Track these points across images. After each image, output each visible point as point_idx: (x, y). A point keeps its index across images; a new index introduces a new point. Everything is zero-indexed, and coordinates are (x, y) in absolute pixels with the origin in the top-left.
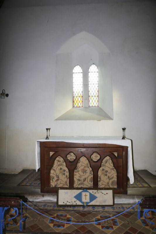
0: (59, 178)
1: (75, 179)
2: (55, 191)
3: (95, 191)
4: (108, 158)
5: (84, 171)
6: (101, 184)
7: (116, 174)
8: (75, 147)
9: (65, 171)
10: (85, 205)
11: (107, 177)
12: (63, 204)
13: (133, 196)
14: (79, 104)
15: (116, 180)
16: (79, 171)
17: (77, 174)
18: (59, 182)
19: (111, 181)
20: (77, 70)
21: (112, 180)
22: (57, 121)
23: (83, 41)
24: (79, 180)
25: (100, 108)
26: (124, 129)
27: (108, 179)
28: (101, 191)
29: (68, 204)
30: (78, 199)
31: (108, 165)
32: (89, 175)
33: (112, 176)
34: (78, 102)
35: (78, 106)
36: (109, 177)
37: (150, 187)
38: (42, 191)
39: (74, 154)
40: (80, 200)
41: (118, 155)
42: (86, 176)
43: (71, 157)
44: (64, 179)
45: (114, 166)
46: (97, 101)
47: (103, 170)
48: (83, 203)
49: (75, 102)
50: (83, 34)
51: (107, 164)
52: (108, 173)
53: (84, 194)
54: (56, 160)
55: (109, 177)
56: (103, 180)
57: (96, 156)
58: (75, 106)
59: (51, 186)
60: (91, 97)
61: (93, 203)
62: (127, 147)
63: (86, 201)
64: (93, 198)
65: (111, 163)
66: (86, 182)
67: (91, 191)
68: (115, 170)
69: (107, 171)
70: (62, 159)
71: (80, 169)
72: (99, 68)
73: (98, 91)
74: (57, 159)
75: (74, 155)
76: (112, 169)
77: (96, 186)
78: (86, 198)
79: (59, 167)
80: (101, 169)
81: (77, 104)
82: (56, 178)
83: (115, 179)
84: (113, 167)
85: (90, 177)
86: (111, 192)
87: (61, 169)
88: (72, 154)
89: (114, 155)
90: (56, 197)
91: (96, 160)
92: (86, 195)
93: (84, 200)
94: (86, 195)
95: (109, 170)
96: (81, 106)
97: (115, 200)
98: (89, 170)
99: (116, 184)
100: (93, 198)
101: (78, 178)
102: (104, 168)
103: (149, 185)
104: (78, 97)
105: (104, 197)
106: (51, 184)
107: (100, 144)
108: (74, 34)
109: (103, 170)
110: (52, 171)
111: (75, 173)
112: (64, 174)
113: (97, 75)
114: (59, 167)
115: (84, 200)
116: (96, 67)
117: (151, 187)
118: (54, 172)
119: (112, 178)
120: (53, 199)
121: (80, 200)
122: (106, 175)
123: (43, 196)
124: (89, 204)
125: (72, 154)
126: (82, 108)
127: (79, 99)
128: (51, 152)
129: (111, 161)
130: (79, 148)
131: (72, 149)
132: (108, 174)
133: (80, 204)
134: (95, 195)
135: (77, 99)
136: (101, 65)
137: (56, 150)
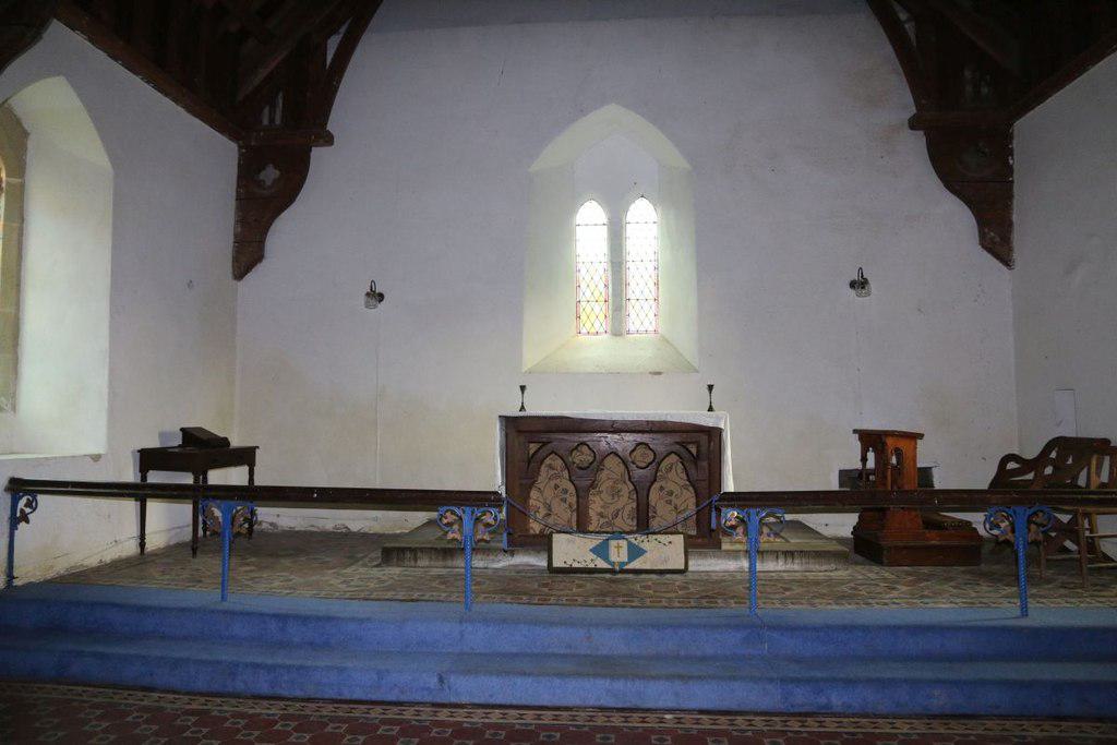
0: (550, 510)
1: (591, 513)
2: (543, 543)
3: (641, 538)
5: (616, 494)
6: (655, 524)
9: (565, 491)
10: (617, 568)
11: (671, 507)
12: (565, 566)
13: (734, 555)
14: (597, 325)
16: (601, 492)
17: (597, 499)
18: (550, 521)
20: (590, 219)
23: (612, 131)
24: (601, 515)
25: (663, 337)
26: (710, 388)
28: (655, 537)
29: (576, 565)
30: (599, 555)
31: (674, 478)
32: (626, 503)
34: (593, 318)
35: (593, 330)
38: (511, 543)
39: (590, 449)
40: (606, 558)
41: (697, 447)
42: (619, 505)
43: (582, 458)
44: (564, 513)
45: (689, 480)
46: (651, 316)
47: (662, 488)
48: (613, 564)
49: (583, 317)
50: (612, 111)
53: (613, 543)
54: (543, 468)
56: (663, 513)
57: (643, 455)
58: (584, 331)
59: (532, 532)
60: (633, 302)
61: (636, 564)
63: (618, 560)
64: (635, 552)
66: (618, 521)
67: (631, 538)
70: (559, 462)
71: (603, 488)
72: (659, 211)
73: (656, 284)
74: (548, 461)
75: (589, 452)
77: (644, 523)
78: (618, 553)
79: (552, 483)
80: (656, 485)
81: (588, 325)
82: (543, 511)
85: (628, 508)
86: (679, 540)
87: (556, 487)
88: (585, 448)
89: (690, 452)
90: (546, 556)
91: (643, 465)
92: (618, 547)
93: (614, 558)
94: (618, 547)
96: (602, 330)
97: (690, 563)
98: (627, 488)
100: (635, 552)
101: (599, 510)
102: (663, 483)
104: (592, 299)
105: (665, 551)
106: (531, 525)
107: (652, 422)
108: (583, 112)
109: (662, 488)
110: (534, 494)
111: (591, 497)
112: (564, 500)
113: (654, 230)
114: (552, 483)
115: (614, 558)
116: (651, 207)
118: (539, 494)
120: (539, 561)
121: (606, 558)
122: (670, 502)
123: (512, 554)
124: (626, 567)
125: (585, 448)
126: (605, 336)
127: (597, 309)
128: (532, 445)
130: (602, 435)
131: (586, 438)
133: (605, 565)
134: (642, 546)
135: (588, 310)
136: (663, 198)
137: (544, 440)
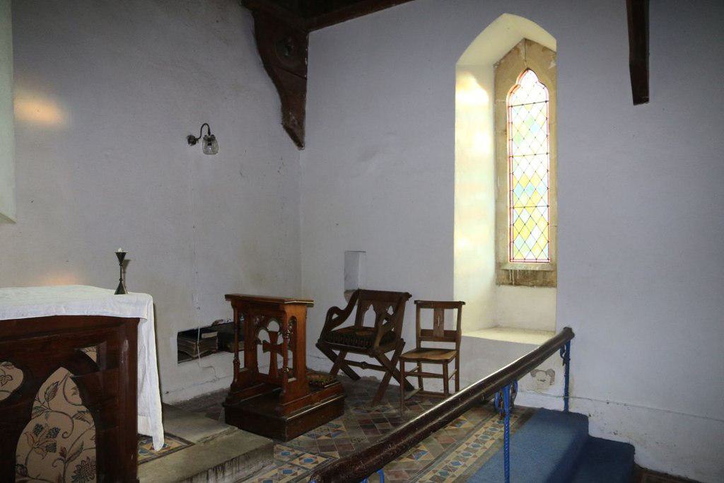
4: (61, 373)
7: (93, 433)
8: (158, 329)
11: (57, 455)
15: (93, 454)
19: (72, 467)
21: (78, 461)
22: (572, 356)
27: (61, 463)
33: (78, 444)
36: (63, 454)
37: (190, 444)
47: (38, 428)
51: (57, 403)
52: (59, 439)
55: (63, 454)
62: (130, 326)
65: (74, 394)
68: (89, 417)
69: (55, 431)
76: (79, 416)
80: (30, 426)
83: (91, 453)
84: (84, 408)
95: (63, 423)
99: (94, 472)
103: (181, 439)
104: (530, 210)
109: (38, 428)
117: (194, 444)
119: (79, 452)
129: (71, 384)
132: (60, 442)
135: (525, 216)
136: (551, 79)
